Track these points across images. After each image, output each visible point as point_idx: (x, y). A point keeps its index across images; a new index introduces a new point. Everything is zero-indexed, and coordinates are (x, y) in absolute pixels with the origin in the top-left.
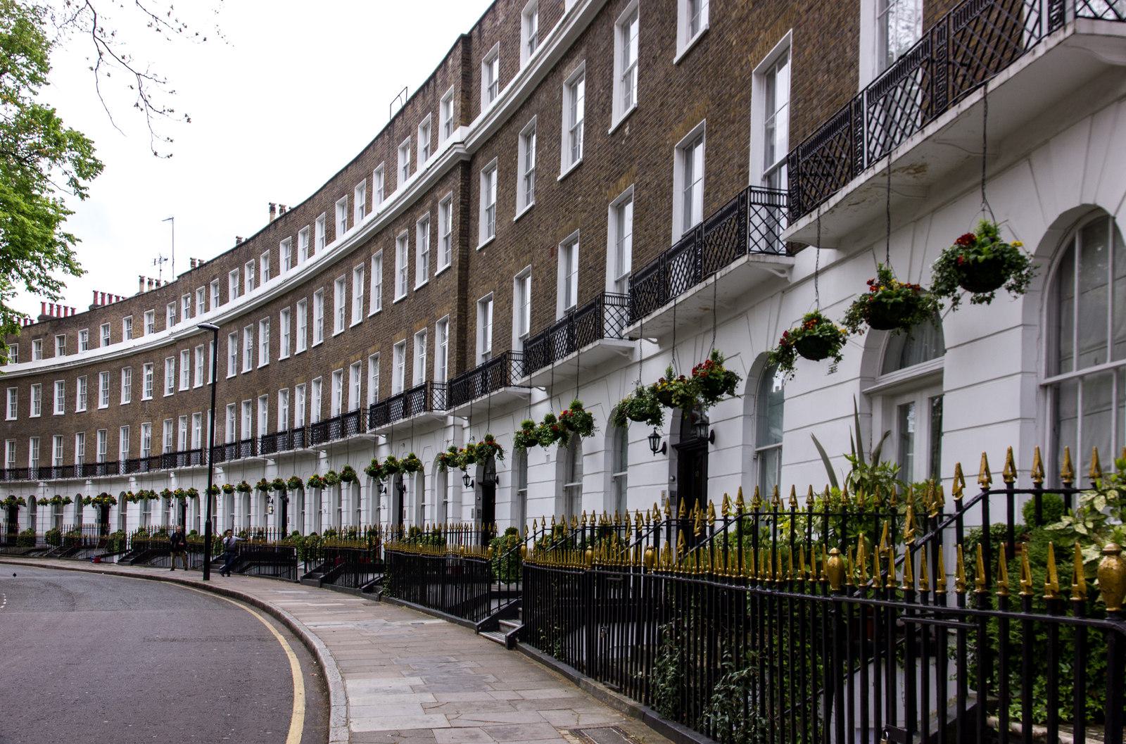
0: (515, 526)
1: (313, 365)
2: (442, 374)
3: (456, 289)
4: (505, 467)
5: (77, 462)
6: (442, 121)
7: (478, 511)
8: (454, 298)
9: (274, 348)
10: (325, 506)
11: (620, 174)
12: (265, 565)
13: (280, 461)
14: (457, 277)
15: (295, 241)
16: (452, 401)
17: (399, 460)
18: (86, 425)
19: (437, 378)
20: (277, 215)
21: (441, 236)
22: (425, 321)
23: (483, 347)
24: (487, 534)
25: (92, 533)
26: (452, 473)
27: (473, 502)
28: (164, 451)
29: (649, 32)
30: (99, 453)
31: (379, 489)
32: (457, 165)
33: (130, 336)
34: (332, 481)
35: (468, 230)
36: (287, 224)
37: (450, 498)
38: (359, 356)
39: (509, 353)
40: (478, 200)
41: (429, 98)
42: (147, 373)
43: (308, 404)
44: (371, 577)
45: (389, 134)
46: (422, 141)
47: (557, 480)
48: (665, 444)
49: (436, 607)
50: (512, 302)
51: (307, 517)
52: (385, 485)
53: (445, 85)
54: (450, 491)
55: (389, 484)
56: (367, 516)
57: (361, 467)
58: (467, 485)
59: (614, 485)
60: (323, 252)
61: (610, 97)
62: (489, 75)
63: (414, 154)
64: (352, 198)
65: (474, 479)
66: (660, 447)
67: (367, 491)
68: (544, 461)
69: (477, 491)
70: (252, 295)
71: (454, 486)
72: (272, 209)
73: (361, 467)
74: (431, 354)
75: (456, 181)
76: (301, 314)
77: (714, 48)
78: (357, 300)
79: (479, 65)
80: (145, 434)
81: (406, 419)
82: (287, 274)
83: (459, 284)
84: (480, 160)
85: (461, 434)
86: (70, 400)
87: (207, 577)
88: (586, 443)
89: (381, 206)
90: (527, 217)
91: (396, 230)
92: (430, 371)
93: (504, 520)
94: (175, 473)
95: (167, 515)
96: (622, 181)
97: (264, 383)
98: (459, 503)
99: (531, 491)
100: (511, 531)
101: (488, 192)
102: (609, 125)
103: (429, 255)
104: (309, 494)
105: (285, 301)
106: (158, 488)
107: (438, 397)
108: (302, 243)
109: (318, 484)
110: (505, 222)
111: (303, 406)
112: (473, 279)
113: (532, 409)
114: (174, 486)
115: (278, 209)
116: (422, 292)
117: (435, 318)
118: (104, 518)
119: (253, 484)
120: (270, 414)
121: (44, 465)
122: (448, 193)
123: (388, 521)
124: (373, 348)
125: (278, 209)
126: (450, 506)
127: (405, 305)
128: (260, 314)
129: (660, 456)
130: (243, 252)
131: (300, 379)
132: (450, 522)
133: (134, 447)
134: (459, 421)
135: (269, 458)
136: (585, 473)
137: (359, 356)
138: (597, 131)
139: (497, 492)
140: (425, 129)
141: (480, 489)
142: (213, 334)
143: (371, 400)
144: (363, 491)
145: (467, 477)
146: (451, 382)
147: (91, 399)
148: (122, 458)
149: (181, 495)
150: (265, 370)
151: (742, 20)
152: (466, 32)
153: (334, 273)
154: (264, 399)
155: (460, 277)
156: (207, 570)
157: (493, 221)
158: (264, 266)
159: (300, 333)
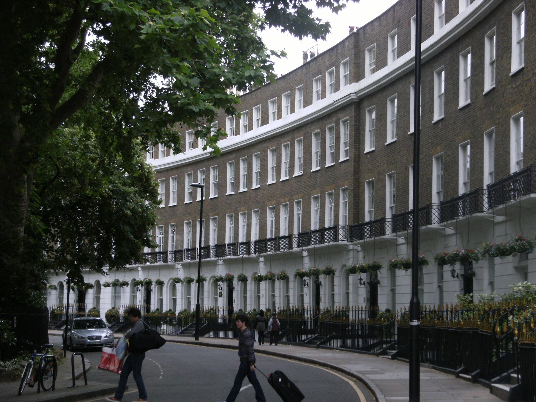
0: (389, 308)
3: (353, 173)
4: (383, 275)
7: (368, 299)
13: (228, 263)
14: (353, 166)
19: (341, 223)
25: (222, 313)
26: (351, 277)
31: (303, 283)
35: (359, 140)
38: (287, 199)
40: (365, 125)
43: (249, 226)
45: (306, 69)
48: (458, 274)
49: (354, 348)
50: (385, 187)
54: (351, 287)
56: (294, 299)
57: (336, 266)
58: (361, 284)
59: (438, 289)
65: (365, 280)
66: (456, 275)
67: (293, 285)
68: (404, 278)
69: (366, 288)
71: (353, 284)
74: (337, 207)
76: (242, 166)
78: (285, 165)
79: (364, 51)
81: (321, 245)
83: (354, 170)
84: (365, 103)
85: (356, 257)
88: (425, 269)
90: (393, 145)
91: (312, 128)
93: (383, 304)
94: (142, 267)
95: (133, 297)
96: (439, 148)
99: (398, 290)
100: (388, 311)
105: (231, 157)
106: (127, 277)
113: (398, 247)
114: (141, 276)
116: (330, 169)
117: (339, 186)
119: (249, 275)
120: (219, 230)
122: (345, 117)
123: (310, 303)
124: (297, 196)
126: (351, 296)
127: (319, 174)
129: (456, 279)
131: (242, 209)
132: (351, 305)
134: (356, 247)
135: (220, 260)
136: (425, 282)
137: (287, 199)
139: (379, 289)
144: (291, 285)
145: (361, 279)
149: (148, 284)
150: (215, 200)
153: (268, 144)
154: (214, 219)
155: (354, 167)
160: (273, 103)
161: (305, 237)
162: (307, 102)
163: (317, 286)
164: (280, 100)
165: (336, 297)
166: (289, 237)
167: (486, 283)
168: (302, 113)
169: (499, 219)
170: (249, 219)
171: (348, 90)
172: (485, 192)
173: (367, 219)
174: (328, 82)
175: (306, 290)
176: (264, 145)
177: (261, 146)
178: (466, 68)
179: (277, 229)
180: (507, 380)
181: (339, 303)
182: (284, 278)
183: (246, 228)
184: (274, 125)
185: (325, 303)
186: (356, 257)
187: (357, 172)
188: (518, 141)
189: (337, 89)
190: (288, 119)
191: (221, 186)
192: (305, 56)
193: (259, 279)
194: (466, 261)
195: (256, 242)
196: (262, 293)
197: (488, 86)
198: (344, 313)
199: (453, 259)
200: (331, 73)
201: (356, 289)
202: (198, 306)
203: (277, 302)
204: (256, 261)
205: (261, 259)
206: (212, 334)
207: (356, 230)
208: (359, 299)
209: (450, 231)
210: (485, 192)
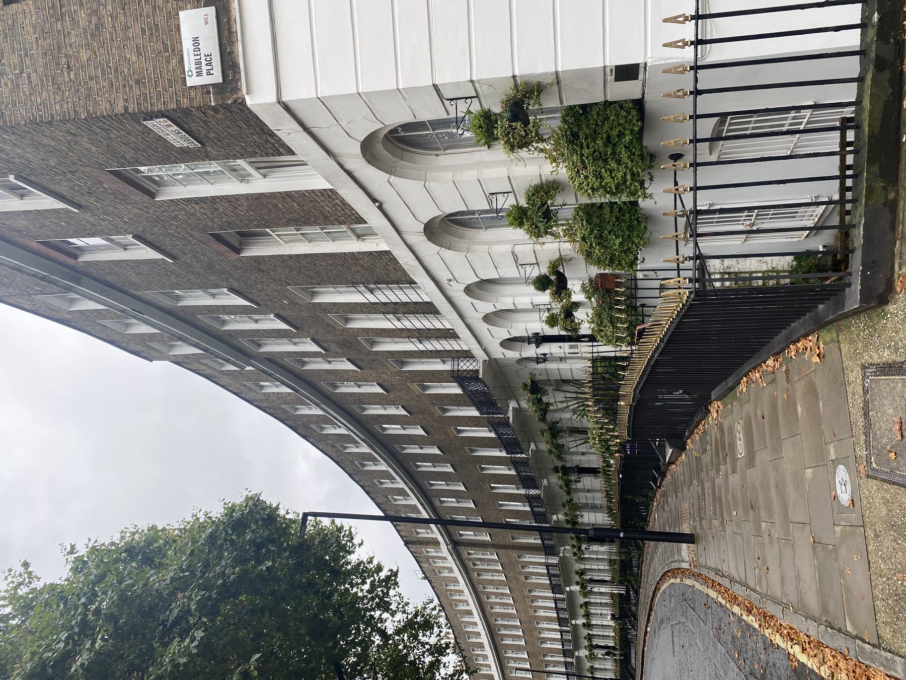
1: (530, 626)
2: (542, 559)
17: (587, 644)
19: (543, 561)
27: (589, 478)
37: (595, 556)
39: (525, 495)
41: (423, 560)
57: (582, 600)
60: (476, 618)
63: (438, 558)
78: (503, 603)
82: (484, 639)
84: (455, 538)
92: (555, 630)
98: (597, 552)
108: (470, 629)
112: (502, 543)
143: (557, 627)
144: (592, 601)
146: (546, 554)
157: (417, 360)
159: (514, 636)
160: (456, 605)
161: (555, 588)
162: (455, 581)
163: (591, 581)
164: (454, 600)
165: (600, 567)
167: (583, 458)
168: (462, 585)
169: (533, 446)
170: (543, 629)
171: (444, 550)
173: (539, 542)
174: (457, 597)
175: (595, 590)
176: (488, 614)
177: (489, 617)
178: (427, 467)
179: (550, 608)
180: (662, 448)
181: (604, 566)
182: (590, 637)
183: (551, 633)
184: (473, 607)
186: (567, 550)
187: (504, 547)
188: (474, 431)
189: (462, 591)
190: (467, 595)
191: (518, 649)
193: (588, 626)
194: (566, 471)
196: (599, 623)
197: (437, 451)
198: (611, 562)
199: (568, 483)
200: (435, 562)
203: (605, 601)
204: (578, 658)
205: (573, 622)
207: (549, 550)
208: (601, 550)
209: (545, 482)
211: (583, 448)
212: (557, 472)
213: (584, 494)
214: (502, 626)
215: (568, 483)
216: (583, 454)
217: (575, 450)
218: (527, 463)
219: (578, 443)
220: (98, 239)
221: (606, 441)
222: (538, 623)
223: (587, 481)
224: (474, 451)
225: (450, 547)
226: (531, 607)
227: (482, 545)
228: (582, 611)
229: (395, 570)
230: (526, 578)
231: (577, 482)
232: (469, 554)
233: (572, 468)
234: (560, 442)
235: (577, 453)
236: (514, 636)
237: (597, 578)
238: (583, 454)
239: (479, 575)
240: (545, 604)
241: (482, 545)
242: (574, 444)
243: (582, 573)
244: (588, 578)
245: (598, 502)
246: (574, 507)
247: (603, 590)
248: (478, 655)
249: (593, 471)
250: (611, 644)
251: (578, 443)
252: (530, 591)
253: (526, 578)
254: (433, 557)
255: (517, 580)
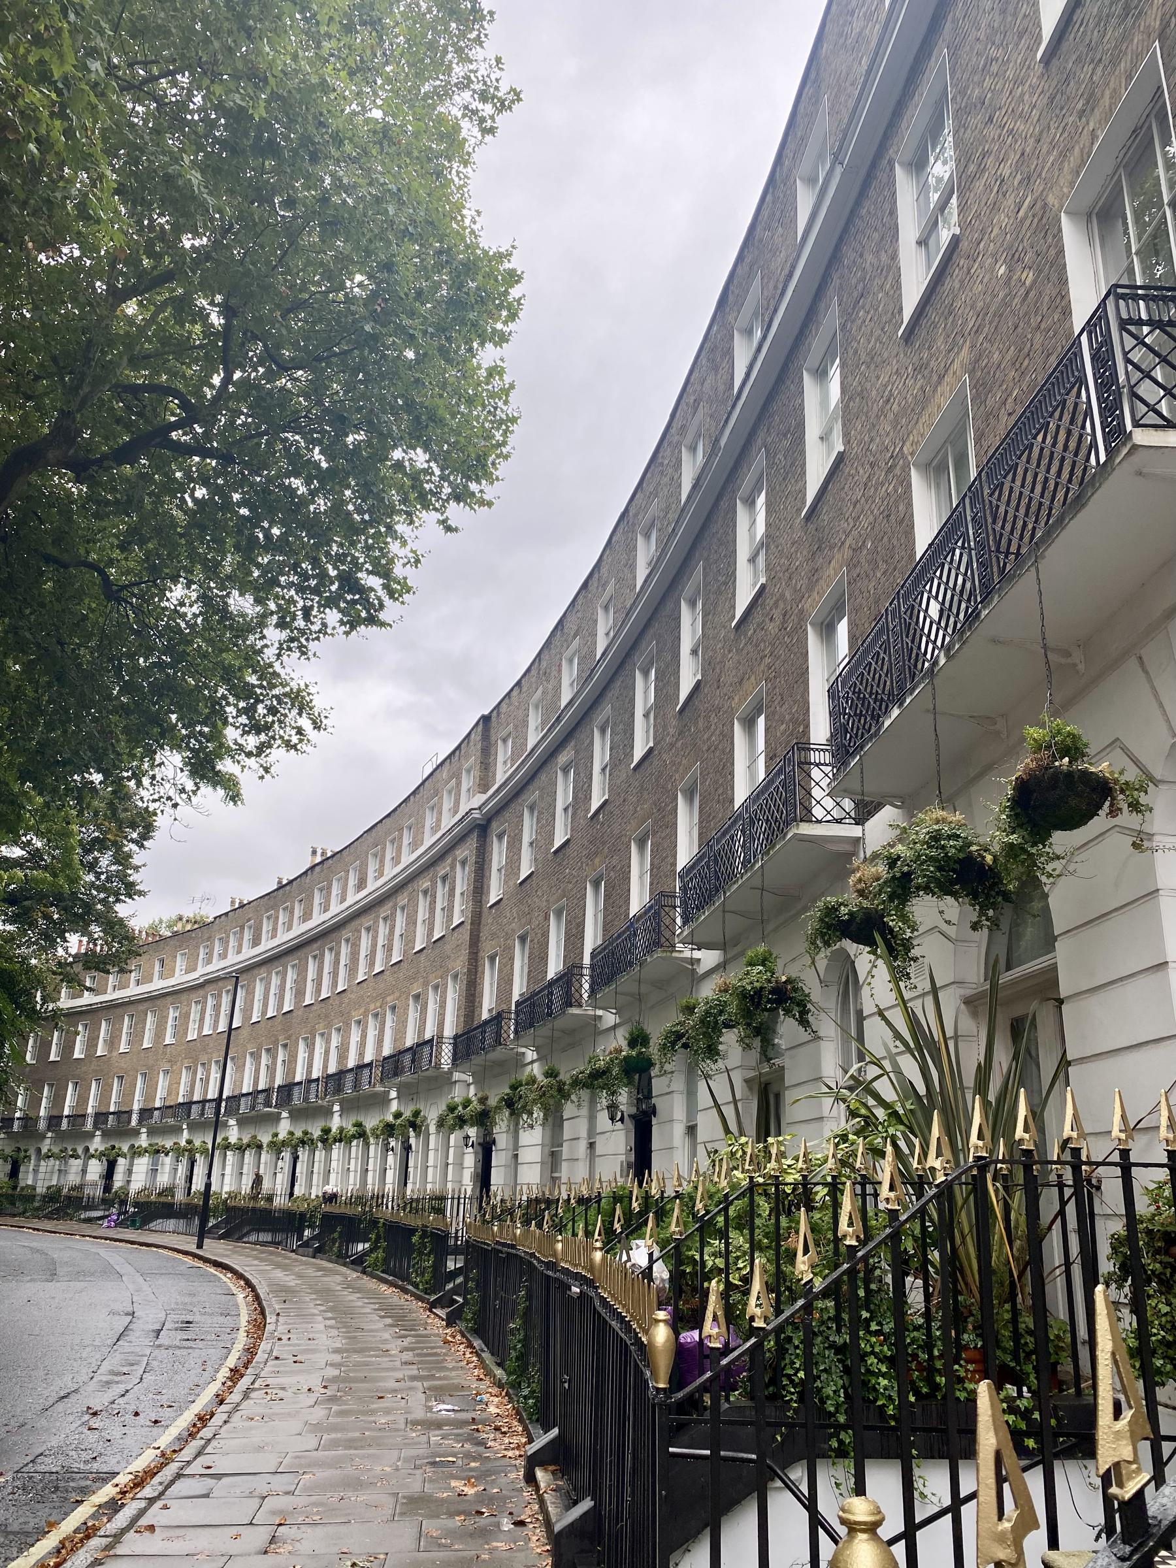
1: (331, 1013)
5: (90, 1110)
6: (464, 786)
8: (464, 953)
9: (300, 993)
10: (334, 1164)
11: (596, 854)
12: (264, 1231)
15: (329, 887)
16: (458, 1058)
18: (102, 1070)
20: (318, 859)
21: (458, 891)
22: (439, 973)
23: (487, 1006)
24: (107, 1188)
27: (622, 1148)
28: (181, 1100)
29: (617, 738)
30: (113, 1100)
32: (470, 831)
33: (161, 977)
34: (343, 1138)
36: (325, 868)
42: (172, 1014)
44: (360, 1247)
46: (447, 805)
47: (542, 1145)
51: (315, 1176)
52: (393, 1144)
53: (467, 757)
55: (287, 1155)
60: (354, 898)
61: (590, 786)
62: (503, 753)
63: (382, 862)
64: (384, 849)
69: (476, 1153)
70: (284, 937)
72: (314, 852)
73: (432, 1114)
74: (442, 1006)
75: (472, 843)
77: (656, 763)
80: (162, 1084)
82: (318, 919)
84: (494, 825)
86: (92, 1043)
87: (200, 1246)
89: (407, 858)
97: (284, 1030)
98: (460, 1165)
101: (498, 855)
102: (588, 810)
103: (443, 911)
104: (320, 1155)
105: (315, 946)
107: (447, 1052)
108: (335, 890)
109: (327, 1139)
110: (511, 883)
111: (315, 1060)
112: (484, 934)
115: (319, 852)
117: (448, 971)
118: (109, 1175)
119: (265, 1139)
121: (55, 1113)
125: (319, 852)
127: (423, 956)
128: (290, 958)
130: (284, 894)
133: (150, 1094)
138: (581, 813)
140: (450, 792)
141: (480, 1149)
142: (238, 977)
146: (456, 1037)
147: (112, 1043)
148: (136, 1107)
151: (672, 745)
152: (486, 713)
156: (201, 1236)
158: (297, 912)
166: (268, 1091)
167: (679, 1130)
170: (328, 1041)
172: (586, 972)
175: (390, 1158)
185: (414, 1183)
186: (464, 1088)
192: (233, 902)
194: (637, 1070)
195: (228, 1098)
199: (596, 1080)
201: (460, 1156)
202: (208, 1186)
203: (370, 1181)
206: (157, 1224)
210: (586, 972)
211: (708, 1126)
212: (632, 1043)
213: (584, 1133)
214: (338, 955)
215: (596, 1080)
216: (691, 1130)
217: (703, 1098)
218: (658, 944)
219: (729, 1112)
220: (846, 651)
221: (747, 1220)
222: (339, 1030)
223: (616, 1142)
224: (690, 799)
225: (476, 815)
226: (365, 1015)
227: (479, 888)
228: (56, 1150)
229: (382, 616)
230: (417, 997)
231: (612, 1108)
232: (463, 863)
233: (649, 1096)
234: (730, 1040)
235: (692, 1108)
236: (325, 977)
237: (411, 1164)
238: (691, 1130)
239: (425, 892)
240: (369, 1043)
241: (479, 888)
242: (724, 1096)
243: (415, 1123)
244: (412, 1141)
245: (564, 1173)
246: (553, 1098)
247: (390, 1174)
248: (292, 913)
249: (641, 1161)
250: (298, 1191)
251: (729, 1112)
252: (393, 1008)
253: (417, 997)
254: (459, 784)
255: (413, 979)
